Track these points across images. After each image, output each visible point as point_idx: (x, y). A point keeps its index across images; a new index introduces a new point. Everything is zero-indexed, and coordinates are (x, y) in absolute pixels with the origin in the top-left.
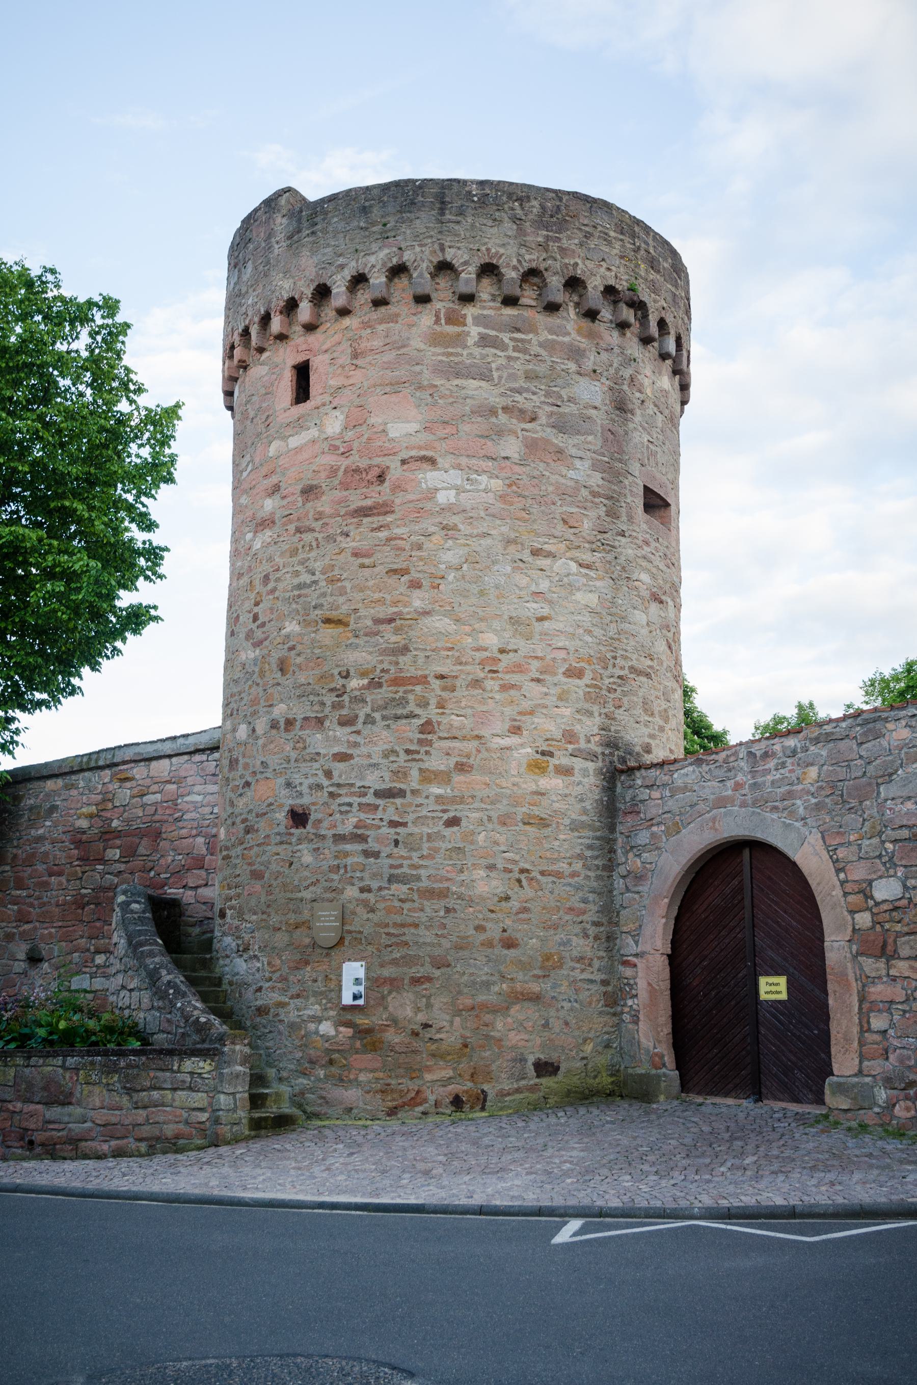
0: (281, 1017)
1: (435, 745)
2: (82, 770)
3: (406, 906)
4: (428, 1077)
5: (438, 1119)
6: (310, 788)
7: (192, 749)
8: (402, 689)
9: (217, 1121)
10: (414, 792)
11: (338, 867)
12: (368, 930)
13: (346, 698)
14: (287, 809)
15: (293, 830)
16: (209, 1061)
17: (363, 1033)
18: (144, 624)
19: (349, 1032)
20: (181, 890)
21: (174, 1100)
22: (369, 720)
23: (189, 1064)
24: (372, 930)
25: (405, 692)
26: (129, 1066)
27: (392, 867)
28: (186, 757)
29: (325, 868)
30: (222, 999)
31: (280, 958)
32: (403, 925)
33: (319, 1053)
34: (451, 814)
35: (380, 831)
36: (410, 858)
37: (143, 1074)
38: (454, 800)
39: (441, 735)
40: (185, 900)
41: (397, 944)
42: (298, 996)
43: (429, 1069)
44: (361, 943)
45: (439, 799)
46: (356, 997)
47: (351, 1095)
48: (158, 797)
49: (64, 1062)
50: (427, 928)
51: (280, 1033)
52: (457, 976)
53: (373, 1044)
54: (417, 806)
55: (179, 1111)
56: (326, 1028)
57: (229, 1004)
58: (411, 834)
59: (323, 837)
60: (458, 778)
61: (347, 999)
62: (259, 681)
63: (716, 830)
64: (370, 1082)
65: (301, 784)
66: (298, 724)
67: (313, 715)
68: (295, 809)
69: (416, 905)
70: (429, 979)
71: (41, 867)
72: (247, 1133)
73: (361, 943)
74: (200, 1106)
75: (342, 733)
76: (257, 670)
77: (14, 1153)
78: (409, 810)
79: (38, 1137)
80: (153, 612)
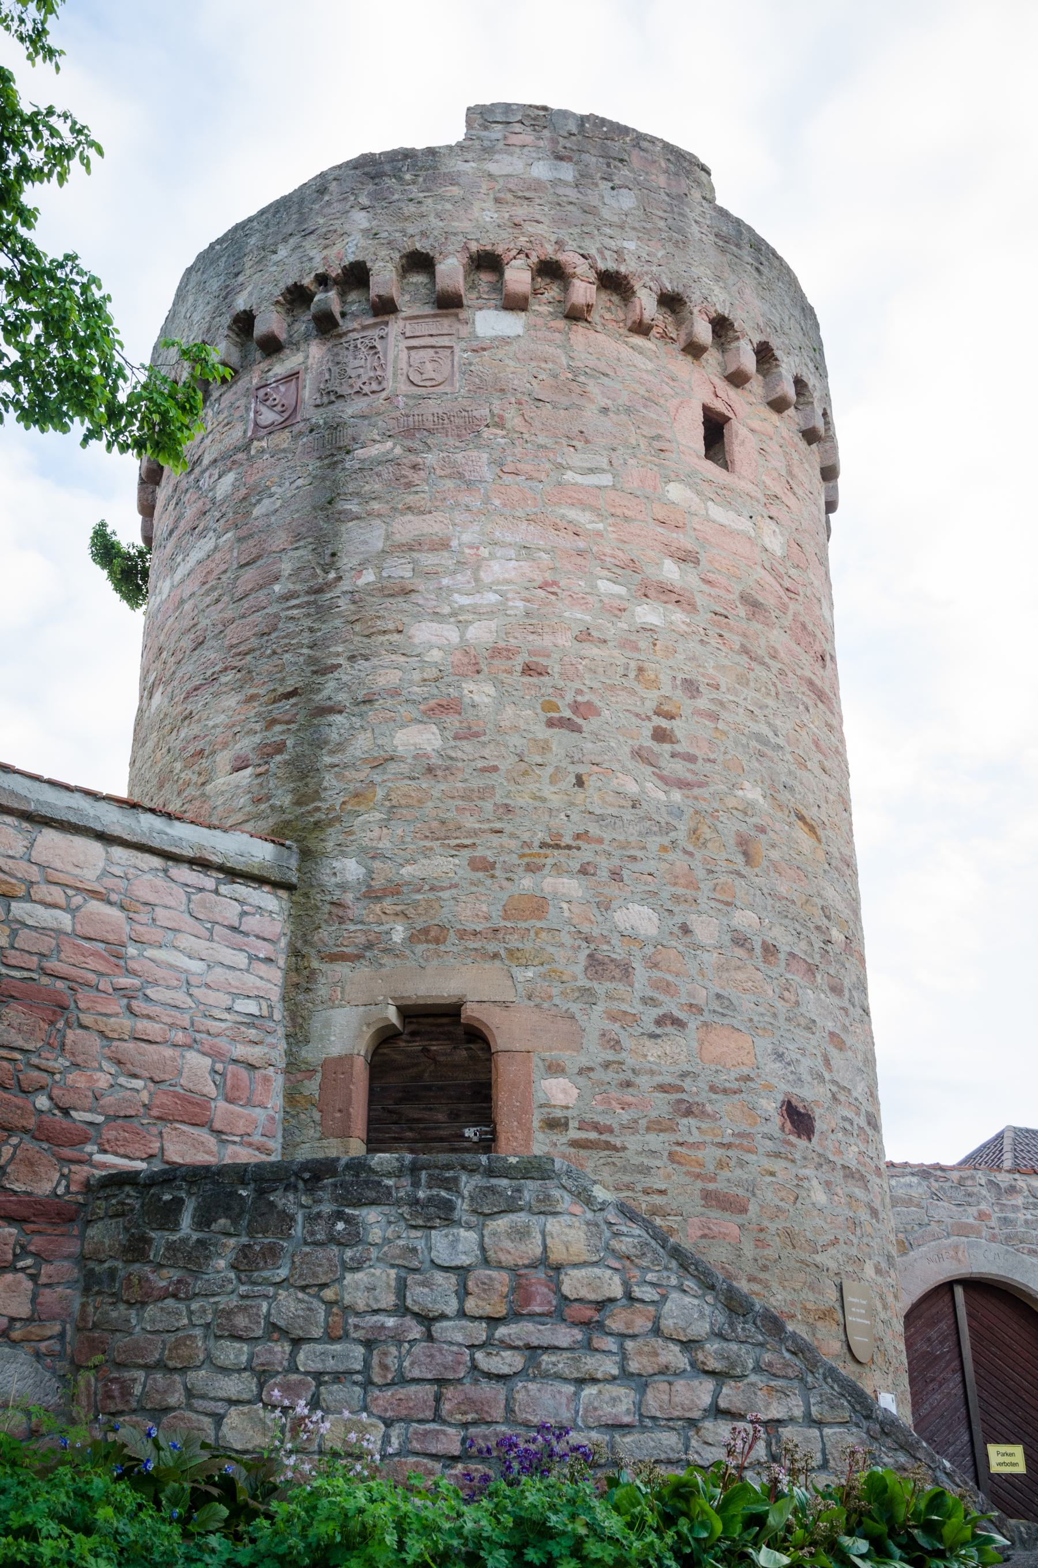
7: (189, 853)
14: (780, 1097)
28: (156, 862)
63: (959, 1261)
68: (794, 1102)
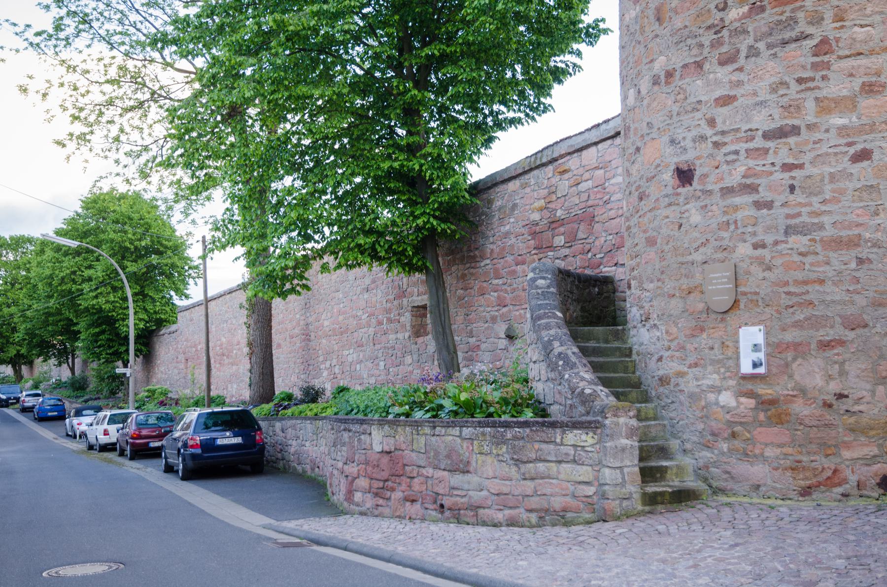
0: (682, 387)
1: (835, 67)
2: (531, 170)
3: (809, 259)
4: (847, 454)
5: (862, 502)
6: (694, 141)
8: (788, 8)
9: (604, 496)
10: (809, 127)
11: (728, 223)
12: (765, 290)
13: (725, 33)
14: (673, 167)
15: (680, 190)
16: (591, 434)
17: (766, 403)
18: (597, 37)
19: (751, 403)
20: (614, 268)
21: (559, 473)
22: (753, 53)
23: (572, 437)
24: (770, 290)
25: (793, 11)
26: (515, 438)
27: (788, 216)
28: (609, 142)
29: (715, 226)
30: (631, 369)
31: (676, 324)
32: (805, 283)
33: (720, 426)
34: (859, 147)
35: (772, 178)
36: (810, 205)
37: (529, 446)
38: (861, 130)
39: (841, 53)
40: (617, 278)
41: (800, 304)
42: (696, 365)
43: (848, 446)
44: (757, 305)
45: (842, 131)
46: (755, 365)
47: (758, 471)
48: (590, 184)
49: (461, 432)
50: (835, 284)
51: (681, 403)
52: (877, 338)
53: (779, 416)
54: (815, 143)
55: (565, 484)
56: (726, 398)
57: (638, 373)
58: (809, 177)
59: (710, 192)
60: (866, 103)
61: (746, 368)
62: (641, 39)
64: (777, 458)
65: (684, 138)
66: (678, 74)
67: (692, 61)
68: (681, 166)
69: (820, 258)
70: (841, 343)
71: (510, 258)
72: (640, 507)
73: (757, 305)
74: (585, 480)
75: (723, 73)
76: (638, 28)
77: (430, 515)
78: (805, 149)
79: (447, 502)
80: (602, 26)
